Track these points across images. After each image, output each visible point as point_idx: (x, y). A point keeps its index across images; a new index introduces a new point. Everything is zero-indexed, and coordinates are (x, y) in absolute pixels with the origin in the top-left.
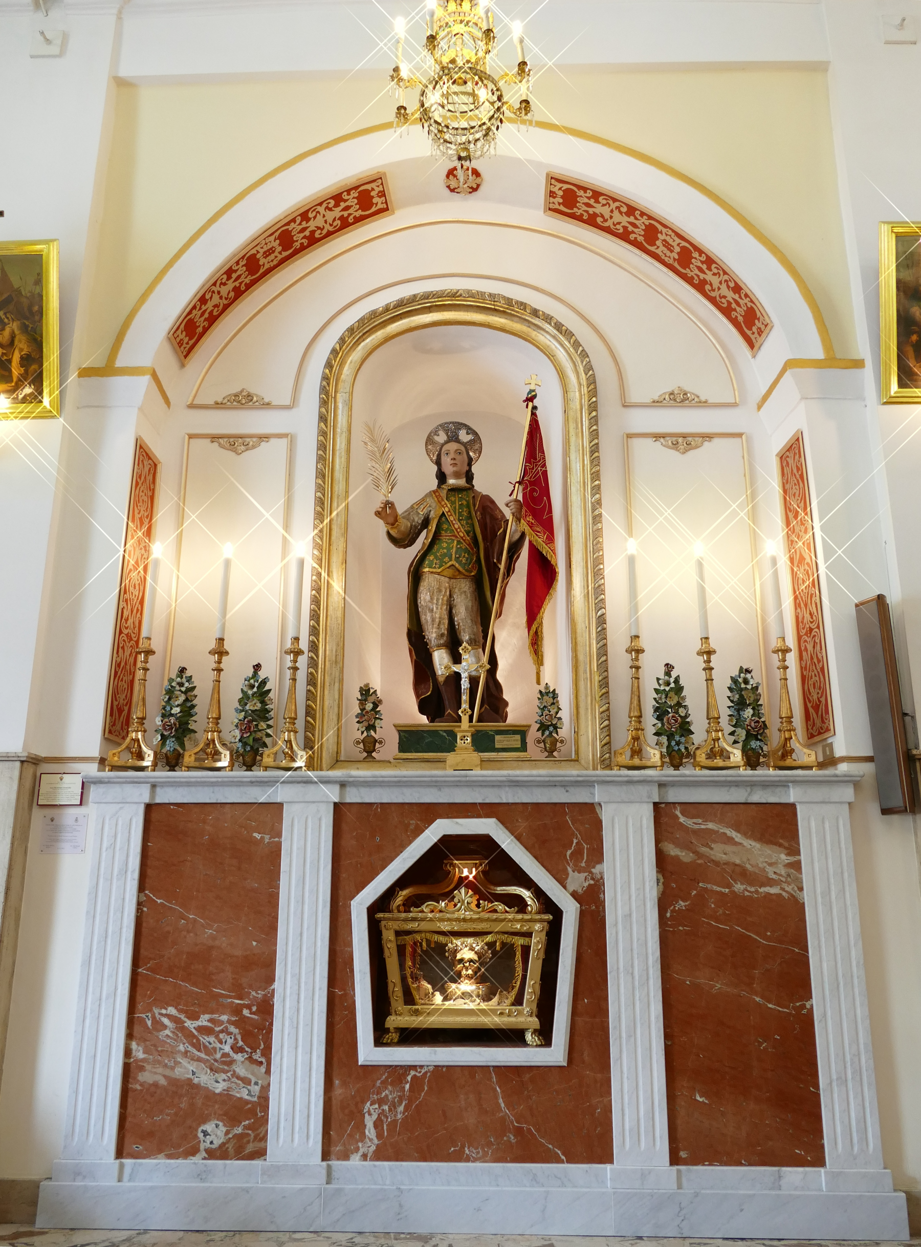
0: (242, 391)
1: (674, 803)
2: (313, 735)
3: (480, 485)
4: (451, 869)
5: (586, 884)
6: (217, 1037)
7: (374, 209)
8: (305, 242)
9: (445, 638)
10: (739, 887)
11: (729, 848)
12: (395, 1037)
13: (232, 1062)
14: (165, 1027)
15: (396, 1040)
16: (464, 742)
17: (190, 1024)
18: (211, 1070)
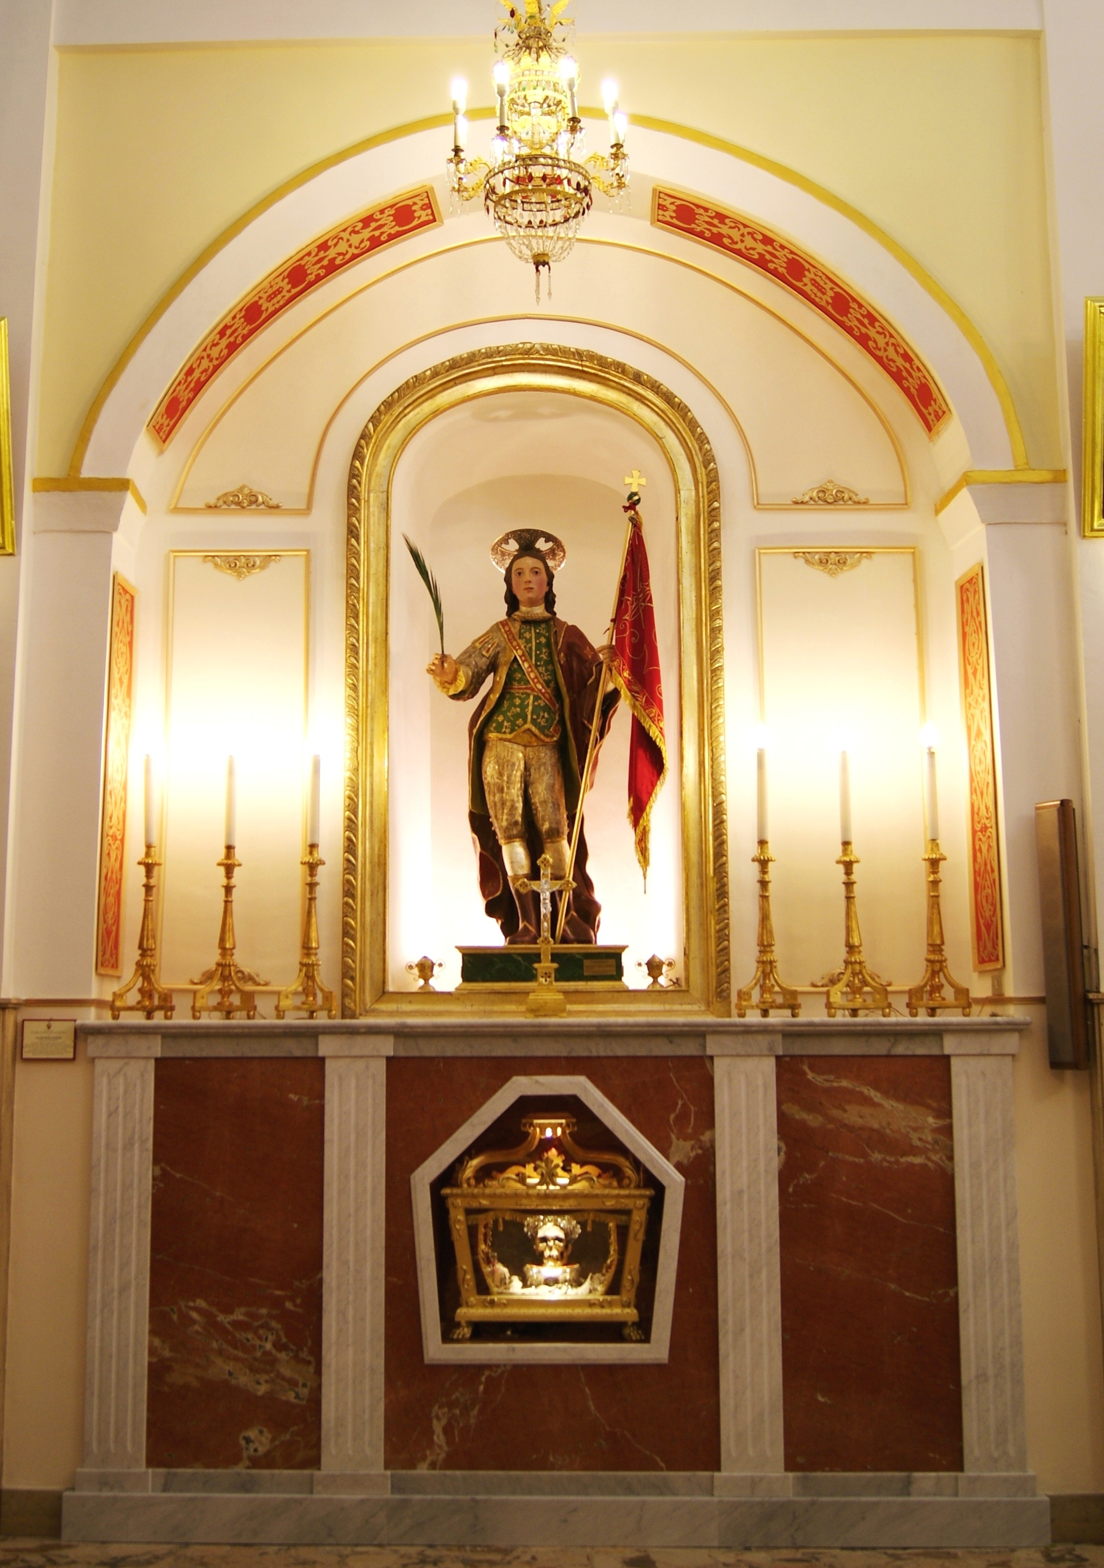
0: (241, 489)
1: (801, 1056)
2: (353, 961)
3: (564, 612)
4: (531, 1130)
5: (693, 1154)
6: (256, 1333)
7: (415, 223)
8: (322, 272)
9: (519, 828)
10: (876, 1156)
11: (866, 1110)
12: (467, 1332)
13: (274, 1361)
14: (194, 1322)
15: (468, 1335)
16: (546, 965)
17: (221, 1318)
18: (251, 1370)
